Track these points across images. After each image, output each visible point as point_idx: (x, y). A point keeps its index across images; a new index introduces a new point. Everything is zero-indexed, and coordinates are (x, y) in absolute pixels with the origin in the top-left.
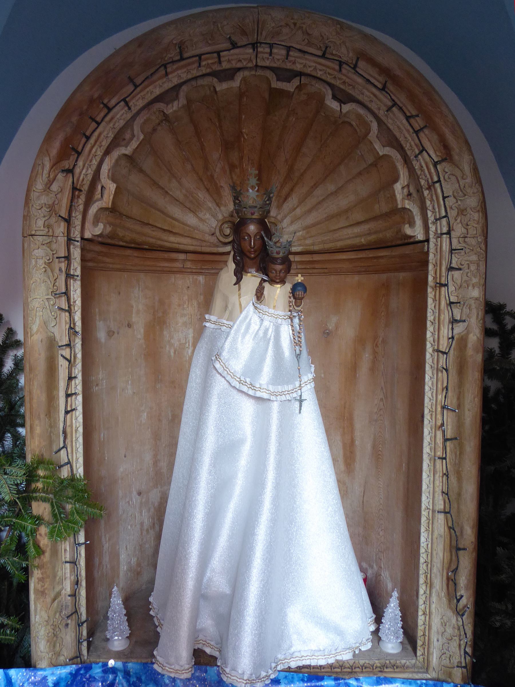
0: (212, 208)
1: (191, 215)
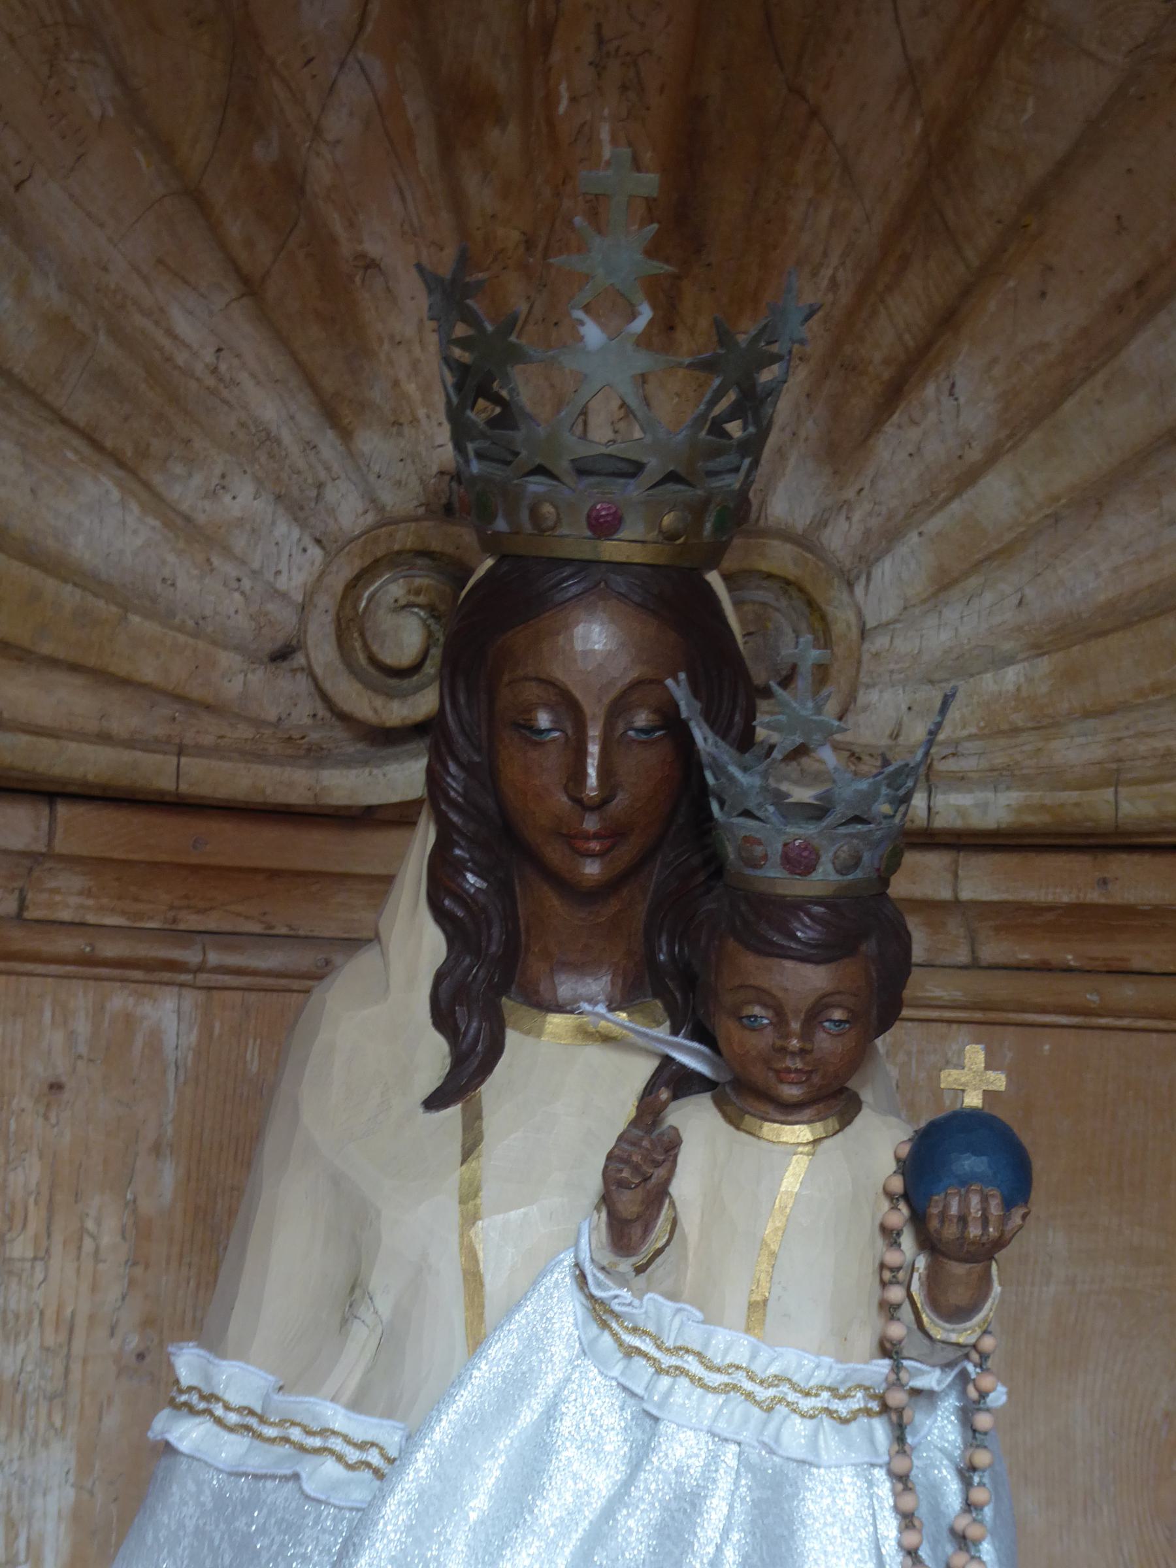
0: (286, 436)
1: (100, 487)
